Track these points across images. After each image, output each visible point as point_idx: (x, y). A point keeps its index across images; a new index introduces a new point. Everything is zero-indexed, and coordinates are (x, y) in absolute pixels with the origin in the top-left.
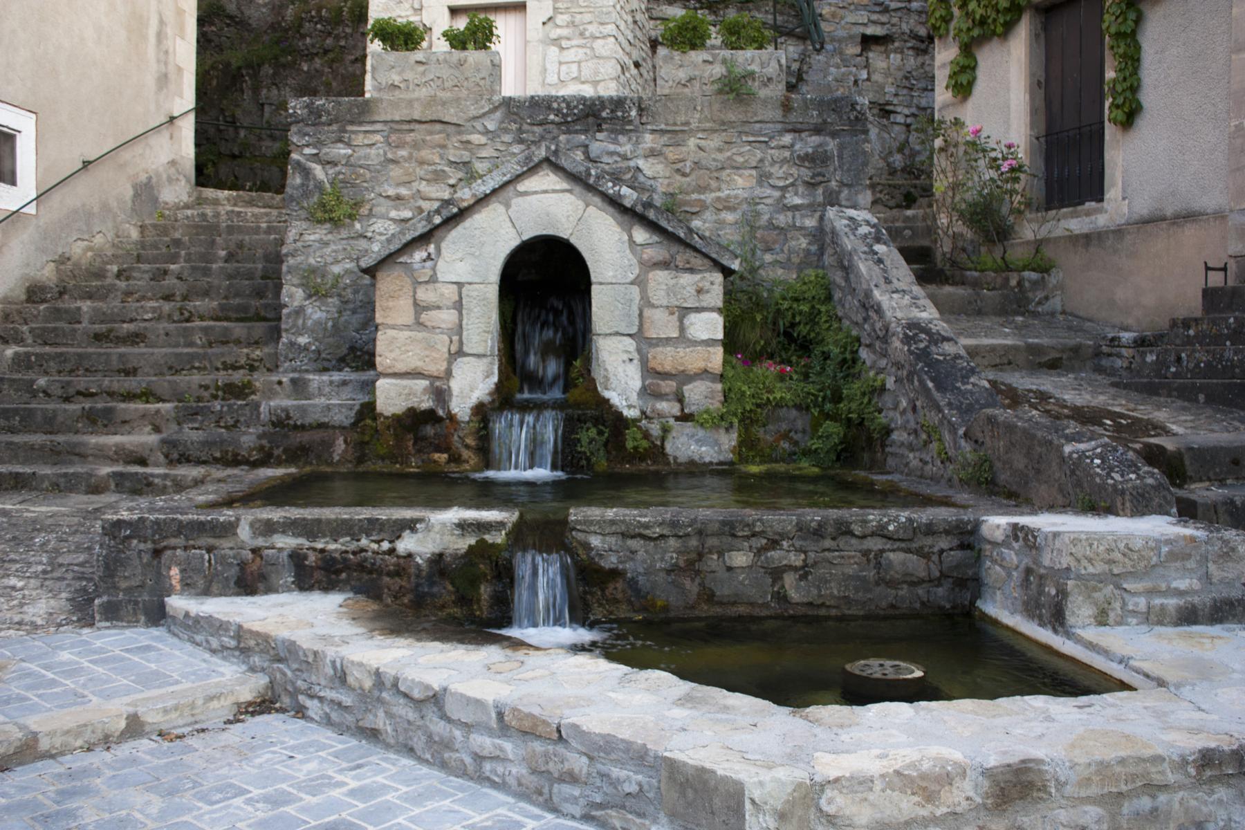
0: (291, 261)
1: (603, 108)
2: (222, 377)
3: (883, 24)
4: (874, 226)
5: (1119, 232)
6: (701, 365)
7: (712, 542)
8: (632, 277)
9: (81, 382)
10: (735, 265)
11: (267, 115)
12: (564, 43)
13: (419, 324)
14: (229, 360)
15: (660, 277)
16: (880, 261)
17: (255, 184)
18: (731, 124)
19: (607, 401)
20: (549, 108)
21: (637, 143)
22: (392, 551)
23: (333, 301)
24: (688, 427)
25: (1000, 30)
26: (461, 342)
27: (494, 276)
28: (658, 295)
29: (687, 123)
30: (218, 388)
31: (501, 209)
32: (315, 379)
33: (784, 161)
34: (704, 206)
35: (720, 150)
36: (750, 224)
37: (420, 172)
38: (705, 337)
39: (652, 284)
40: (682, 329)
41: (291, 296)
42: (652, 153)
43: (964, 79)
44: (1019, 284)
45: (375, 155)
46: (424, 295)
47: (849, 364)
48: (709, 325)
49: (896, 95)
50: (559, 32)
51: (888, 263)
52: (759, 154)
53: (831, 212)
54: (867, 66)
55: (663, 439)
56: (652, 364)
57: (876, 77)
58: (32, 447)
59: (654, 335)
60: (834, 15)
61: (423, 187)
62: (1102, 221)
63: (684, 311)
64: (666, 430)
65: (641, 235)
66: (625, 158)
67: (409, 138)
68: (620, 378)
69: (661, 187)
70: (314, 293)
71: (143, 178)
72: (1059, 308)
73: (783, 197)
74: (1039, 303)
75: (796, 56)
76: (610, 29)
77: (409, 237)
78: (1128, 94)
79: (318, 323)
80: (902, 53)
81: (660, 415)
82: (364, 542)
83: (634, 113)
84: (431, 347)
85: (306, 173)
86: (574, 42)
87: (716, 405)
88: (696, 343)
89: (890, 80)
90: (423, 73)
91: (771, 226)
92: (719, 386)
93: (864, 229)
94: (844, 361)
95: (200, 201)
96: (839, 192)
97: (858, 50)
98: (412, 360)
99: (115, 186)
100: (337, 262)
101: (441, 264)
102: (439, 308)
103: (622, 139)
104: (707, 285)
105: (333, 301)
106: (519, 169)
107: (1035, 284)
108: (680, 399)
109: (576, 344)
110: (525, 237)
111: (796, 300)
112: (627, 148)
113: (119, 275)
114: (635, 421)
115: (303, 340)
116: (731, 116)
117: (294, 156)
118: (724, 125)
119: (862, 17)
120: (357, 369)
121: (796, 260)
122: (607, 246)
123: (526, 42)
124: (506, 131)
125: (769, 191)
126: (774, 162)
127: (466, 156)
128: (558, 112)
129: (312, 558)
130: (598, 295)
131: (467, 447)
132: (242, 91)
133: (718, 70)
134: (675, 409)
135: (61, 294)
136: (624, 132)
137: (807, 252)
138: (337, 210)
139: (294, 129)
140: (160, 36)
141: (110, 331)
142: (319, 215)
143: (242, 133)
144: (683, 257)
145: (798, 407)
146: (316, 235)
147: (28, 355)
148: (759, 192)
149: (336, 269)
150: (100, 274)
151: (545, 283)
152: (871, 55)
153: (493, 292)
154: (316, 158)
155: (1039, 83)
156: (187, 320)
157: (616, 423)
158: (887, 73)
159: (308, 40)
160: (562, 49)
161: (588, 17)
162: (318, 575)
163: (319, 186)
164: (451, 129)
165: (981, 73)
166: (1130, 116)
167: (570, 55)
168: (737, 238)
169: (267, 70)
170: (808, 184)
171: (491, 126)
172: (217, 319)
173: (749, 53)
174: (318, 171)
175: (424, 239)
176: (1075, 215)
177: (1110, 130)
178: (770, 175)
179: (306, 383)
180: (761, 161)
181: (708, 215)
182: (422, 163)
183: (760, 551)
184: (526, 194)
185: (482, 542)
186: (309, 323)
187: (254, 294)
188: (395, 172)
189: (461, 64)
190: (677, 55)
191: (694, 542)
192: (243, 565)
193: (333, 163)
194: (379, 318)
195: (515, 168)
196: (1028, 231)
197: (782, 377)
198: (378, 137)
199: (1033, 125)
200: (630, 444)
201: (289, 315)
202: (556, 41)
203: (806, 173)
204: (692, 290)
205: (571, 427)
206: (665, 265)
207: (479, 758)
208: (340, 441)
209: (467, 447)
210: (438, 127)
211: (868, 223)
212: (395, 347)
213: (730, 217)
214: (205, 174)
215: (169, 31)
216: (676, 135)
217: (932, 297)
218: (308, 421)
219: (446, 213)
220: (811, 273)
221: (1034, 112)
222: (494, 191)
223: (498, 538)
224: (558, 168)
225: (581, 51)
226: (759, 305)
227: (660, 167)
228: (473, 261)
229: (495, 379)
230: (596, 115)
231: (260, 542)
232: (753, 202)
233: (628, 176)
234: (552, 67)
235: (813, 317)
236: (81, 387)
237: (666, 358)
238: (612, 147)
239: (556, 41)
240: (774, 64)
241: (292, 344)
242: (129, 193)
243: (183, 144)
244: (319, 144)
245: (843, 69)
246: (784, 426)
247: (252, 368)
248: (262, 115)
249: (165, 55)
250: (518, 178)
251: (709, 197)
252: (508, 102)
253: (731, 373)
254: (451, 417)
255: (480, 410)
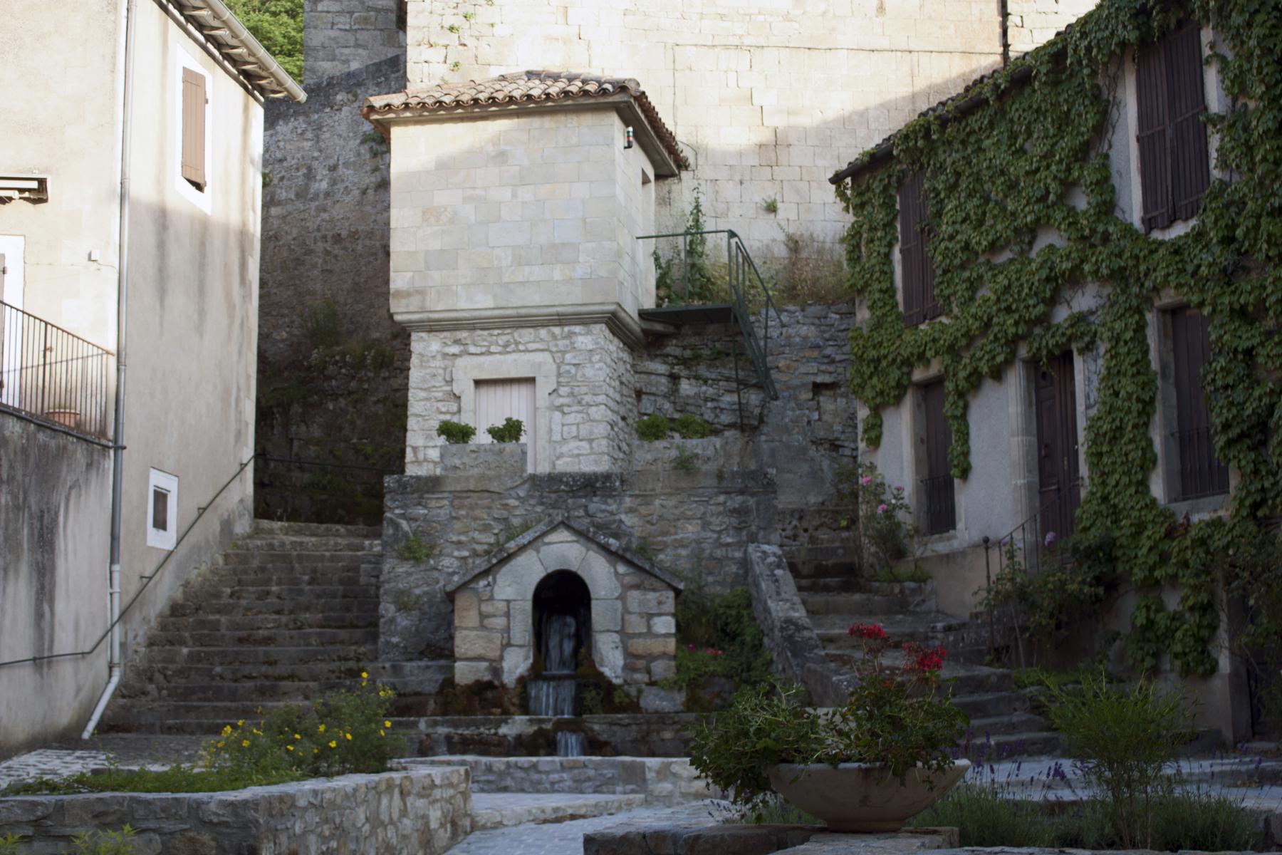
0: (387, 586)
1: (597, 481)
2: (344, 666)
3: (831, 373)
4: (779, 557)
5: (963, 553)
6: (661, 649)
7: (653, 727)
8: (616, 595)
9: (247, 670)
10: (681, 586)
11: (295, 449)
12: (566, 409)
13: (482, 627)
14: (342, 654)
15: (634, 595)
16: (777, 581)
17: (286, 511)
18: (683, 489)
19: (602, 674)
20: (561, 481)
21: (620, 504)
22: (496, 734)
23: (416, 613)
24: (654, 690)
25: (892, 401)
26: (509, 638)
27: (530, 596)
28: (634, 606)
29: (653, 490)
30: (341, 672)
31: (534, 553)
32: (408, 666)
33: (719, 513)
34: (665, 545)
35: (676, 507)
36: (697, 556)
37: (474, 525)
38: (663, 631)
39: (629, 599)
40: (649, 627)
41: (386, 610)
42: (631, 510)
43: (873, 434)
44: (902, 591)
45: (443, 513)
46: (486, 608)
47: (758, 647)
48: (665, 625)
49: (843, 432)
50: (562, 400)
51: (781, 582)
52: (702, 509)
53: (751, 547)
54: (818, 408)
55: (638, 697)
56: (631, 650)
57: (827, 417)
58: (230, 709)
59: (631, 630)
60: (788, 367)
61: (476, 535)
62: (956, 544)
63: (650, 616)
64: (640, 692)
65: (622, 569)
66: (612, 513)
67: (467, 502)
68: (610, 659)
69: (637, 532)
70: (403, 607)
71: (226, 516)
72: (934, 608)
73: (719, 538)
74: (918, 605)
75: (757, 403)
76: (602, 398)
77: (476, 572)
78: (962, 458)
79: (405, 628)
80: (847, 397)
81: (636, 682)
82: (482, 730)
83: (617, 484)
84: (490, 641)
85: (397, 526)
86: (574, 409)
87: (671, 675)
88: (657, 636)
89: (838, 420)
90: (476, 459)
91: (712, 558)
92: (673, 663)
93: (771, 559)
94: (754, 646)
95: (257, 532)
96: (757, 534)
97: (810, 395)
98: (478, 649)
99: (212, 524)
100: (418, 586)
101: (496, 588)
102: (495, 616)
103: (610, 501)
104: (664, 599)
105: (416, 613)
106: (544, 528)
107: (913, 591)
108: (649, 672)
109: (583, 637)
110: (550, 571)
111: (728, 607)
112: (613, 507)
113: (231, 596)
114: (620, 686)
115: (395, 640)
116: (683, 485)
117: (388, 515)
118: (679, 490)
119: (813, 367)
120: (433, 659)
121: (729, 580)
122: (601, 576)
123: (536, 409)
124: (532, 497)
125: (709, 534)
126: (712, 515)
127: (505, 514)
128: (567, 484)
129: (456, 738)
130: (596, 607)
131: (513, 704)
132: (272, 427)
133: (674, 453)
134: (646, 678)
135: (197, 610)
136: (610, 496)
137: (737, 575)
138: (417, 550)
139: (388, 496)
140: (238, 400)
141: (250, 636)
142: (406, 555)
143: (272, 465)
144: (648, 581)
145: (726, 676)
146: (402, 569)
147: (199, 652)
148: (703, 534)
149: (417, 591)
150: (218, 595)
151: (562, 598)
152: (821, 399)
153: (528, 606)
154: (403, 516)
155: (922, 440)
156: (300, 628)
157: (609, 687)
158: (835, 415)
159: (334, 382)
160: (564, 413)
161: (584, 390)
162: (459, 747)
163: (405, 535)
164: (495, 496)
165: (885, 429)
166: (965, 473)
167: (571, 419)
168: (689, 566)
169: (297, 409)
170: (736, 528)
171: (522, 494)
172: (322, 627)
173: (694, 441)
174: (404, 525)
175: (485, 573)
176: (941, 540)
177: (957, 482)
178: (709, 523)
179: (402, 667)
180: (704, 513)
181: (670, 551)
182: (475, 519)
183: (678, 731)
184: (549, 544)
185: (540, 729)
186: (399, 628)
187: (355, 607)
188: (457, 525)
189: (501, 452)
190: (646, 443)
191: (645, 727)
192: (421, 742)
193: (415, 520)
194: (457, 622)
195: (542, 527)
196: (918, 551)
197: (715, 657)
198: (446, 502)
199: (918, 471)
200: (617, 700)
201: (385, 623)
202: (559, 408)
203: (734, 521)
204: (654, 603)
205: (581, 688)
206: (637, 587)
207: (553, 783)
208: (432, 702)
209: (513, 704)
210: (486, 495)
211: (774, 554)
212: (468, 641)
213: (683, 552)
214: (263, 509)
215: (242, 394)
216: (646, 498)
217: (804, 603)
218: (408, 690)
219: (499, 557)
220: (739, 589)
221: (918, 462)
222: (530, 543)
223: (549, 726)
224: (569, 528)
225: (579, 416)
226: (704, 611)
227: (636, 520)
228: (516, 585)
229: (531, 661)
230: (592, 486)
231: (430, 730)
232: (699, 542)
233: (614, 526)
234: (557, 428)
235: (739, 618)
236: (246, 672)
237: (639, 646)
238: (603, 507)
239: (559, 408)
240: (711, 448)
241: (388, 642)
242: (218, 528)
243: (246, 487)
244: (404, 507)
245: (798, 412)
246: (717, 689)
247: (359, 660)
248: (291, 449)
249: (240, 413)
250: (544, 534)
251: (669, 539)
252: (533, 478)
253: (680, 654)
254: (503, 686)
255: (522, 681)
